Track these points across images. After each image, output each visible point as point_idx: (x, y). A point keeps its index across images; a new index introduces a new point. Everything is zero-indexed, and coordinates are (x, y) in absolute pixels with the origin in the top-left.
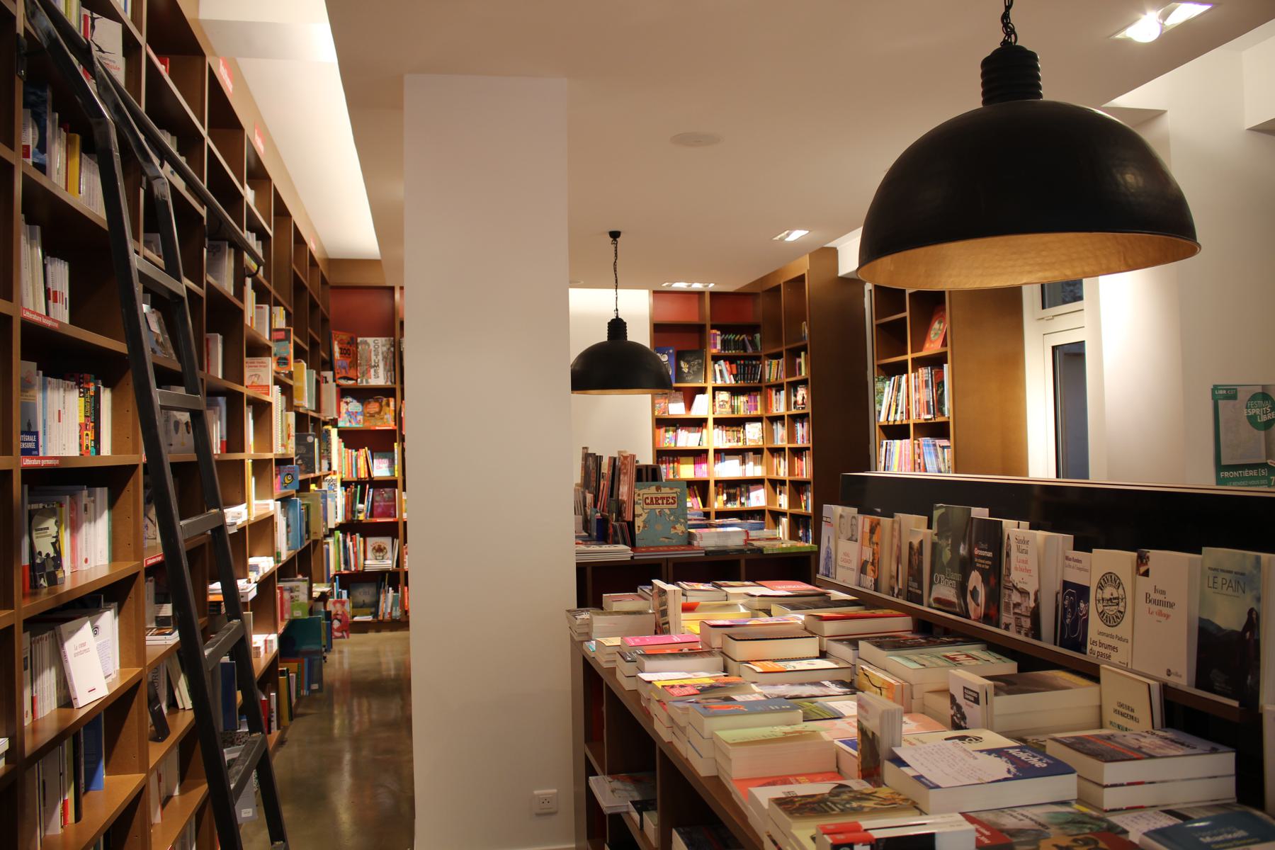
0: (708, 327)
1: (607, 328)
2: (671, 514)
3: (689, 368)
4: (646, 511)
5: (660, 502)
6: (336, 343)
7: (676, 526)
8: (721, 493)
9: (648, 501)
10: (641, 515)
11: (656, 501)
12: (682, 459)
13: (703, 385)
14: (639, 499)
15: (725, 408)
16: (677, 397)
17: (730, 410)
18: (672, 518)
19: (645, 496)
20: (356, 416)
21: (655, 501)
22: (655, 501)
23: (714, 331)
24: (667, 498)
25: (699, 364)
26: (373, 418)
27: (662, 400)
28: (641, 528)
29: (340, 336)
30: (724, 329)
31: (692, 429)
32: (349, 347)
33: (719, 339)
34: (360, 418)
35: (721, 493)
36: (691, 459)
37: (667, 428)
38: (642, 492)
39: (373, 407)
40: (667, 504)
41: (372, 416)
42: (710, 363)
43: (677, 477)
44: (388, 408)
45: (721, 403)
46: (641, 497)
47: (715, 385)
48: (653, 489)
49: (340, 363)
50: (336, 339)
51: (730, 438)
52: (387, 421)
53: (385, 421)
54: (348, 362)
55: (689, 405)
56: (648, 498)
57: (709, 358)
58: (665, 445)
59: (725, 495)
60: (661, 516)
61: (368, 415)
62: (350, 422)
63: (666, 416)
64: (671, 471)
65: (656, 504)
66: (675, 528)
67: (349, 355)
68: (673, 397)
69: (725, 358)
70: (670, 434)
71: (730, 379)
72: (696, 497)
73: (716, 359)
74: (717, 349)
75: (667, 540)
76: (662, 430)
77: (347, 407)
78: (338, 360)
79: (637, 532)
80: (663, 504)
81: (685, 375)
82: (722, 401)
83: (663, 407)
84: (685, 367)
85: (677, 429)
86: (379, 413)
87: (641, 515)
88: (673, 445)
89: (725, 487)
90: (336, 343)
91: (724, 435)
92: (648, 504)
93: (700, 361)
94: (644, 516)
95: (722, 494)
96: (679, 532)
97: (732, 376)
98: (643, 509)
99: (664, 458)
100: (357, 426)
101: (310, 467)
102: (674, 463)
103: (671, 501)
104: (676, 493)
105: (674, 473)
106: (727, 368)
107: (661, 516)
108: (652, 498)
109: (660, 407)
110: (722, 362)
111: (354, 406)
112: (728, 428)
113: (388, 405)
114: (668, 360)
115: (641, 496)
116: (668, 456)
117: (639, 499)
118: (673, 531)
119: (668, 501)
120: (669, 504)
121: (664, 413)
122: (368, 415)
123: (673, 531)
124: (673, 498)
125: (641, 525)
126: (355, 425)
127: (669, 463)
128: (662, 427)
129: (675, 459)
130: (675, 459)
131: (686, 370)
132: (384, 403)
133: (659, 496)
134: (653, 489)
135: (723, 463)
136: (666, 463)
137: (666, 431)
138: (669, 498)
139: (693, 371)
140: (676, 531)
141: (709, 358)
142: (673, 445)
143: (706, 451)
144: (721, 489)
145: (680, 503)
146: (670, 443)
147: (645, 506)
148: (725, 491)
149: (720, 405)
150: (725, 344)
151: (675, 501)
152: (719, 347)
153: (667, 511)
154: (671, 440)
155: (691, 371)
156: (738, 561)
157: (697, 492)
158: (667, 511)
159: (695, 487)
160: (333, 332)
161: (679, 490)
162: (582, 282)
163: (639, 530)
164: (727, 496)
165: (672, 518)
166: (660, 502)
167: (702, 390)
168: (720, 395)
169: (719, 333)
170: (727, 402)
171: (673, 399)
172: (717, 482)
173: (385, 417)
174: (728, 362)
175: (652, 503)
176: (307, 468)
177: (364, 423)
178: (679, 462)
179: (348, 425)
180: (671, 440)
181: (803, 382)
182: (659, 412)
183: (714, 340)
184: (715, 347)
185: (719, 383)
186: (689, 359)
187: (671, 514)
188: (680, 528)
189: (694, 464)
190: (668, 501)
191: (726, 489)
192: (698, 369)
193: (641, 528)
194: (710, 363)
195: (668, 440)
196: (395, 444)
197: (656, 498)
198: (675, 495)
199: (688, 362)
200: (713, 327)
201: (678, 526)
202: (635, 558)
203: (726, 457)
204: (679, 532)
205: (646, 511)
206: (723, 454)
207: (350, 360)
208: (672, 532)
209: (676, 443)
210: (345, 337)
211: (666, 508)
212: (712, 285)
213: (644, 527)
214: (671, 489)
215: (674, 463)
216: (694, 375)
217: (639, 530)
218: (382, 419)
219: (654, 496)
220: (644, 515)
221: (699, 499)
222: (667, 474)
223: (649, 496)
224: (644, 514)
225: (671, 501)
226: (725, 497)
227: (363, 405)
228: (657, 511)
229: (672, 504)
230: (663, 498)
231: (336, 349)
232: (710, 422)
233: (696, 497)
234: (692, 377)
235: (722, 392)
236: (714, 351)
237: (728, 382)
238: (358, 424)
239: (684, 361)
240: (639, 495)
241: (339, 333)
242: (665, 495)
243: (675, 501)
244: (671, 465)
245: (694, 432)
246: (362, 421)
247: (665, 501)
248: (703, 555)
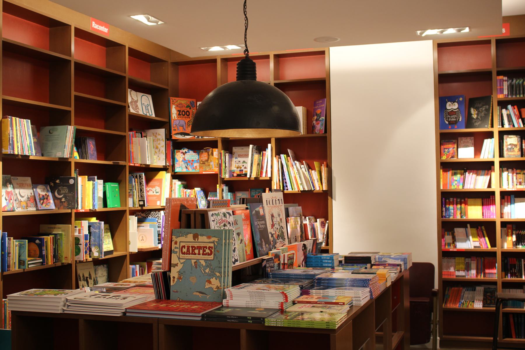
0: (494, 74)
1: (257, 72)
2: (207, 266)
3: (478, 114)
4: (182, 261)
5: (196, 251)
6: (174, 106)
7: (211, 280)
8: (510, 233)
9: (185, 250)
10: (177, 265)
11: (193, 250)
12: (470, 201)
13: (490, 129)
14: (176, 248)
15: (513, 151)
16: (468, 142)
17: (519, 153)
18: (207, 271)
19: (182, 244)
20: (192, 164)
21: (191, 250)
22: (191, 250)
23: (501, 77)
24: (204, 247)
25: (486, 110)
26: (204, 165)
27: (450, 146)
28: (176, 280)
29: (179, 101)
30: (511, 74)
31: (481, 172)
32: (188, 109)
33: (506, 85)
34: (196, 164)
35: (510, 233)
36: (479, 201)
37: (456, 171)
38: (179, 240)
39: (204, 156)
40: (203, 254)
41: (204, 163)
42: (496, 109)
43: (464, 218)
44: (212, 157)
45: (510, 147)
46: (178, 246)
47: (502, 129)
48: (190, 237)
49: (177, 122)
50: (173, 104)
51: (521, 180)
52: (212, 167)
53: (211, 167)
54: (187, 122)
55: (478, 150)
56: (184, 247)
57: (495, 104)
58: (453, 188)
59: (514, 236)
60: (196, 267)
61: (202, 162)
62: (187, 168)
63: (455, 160)
64: (458, 212)
65: (192, 254)
66: (210, 282)
67: (189, 115)
68: (464, 142)
69: (513, 103)
70: (458, 177)
71: (518, 123)
72: (484, 237)
73: (503, 104)
74: (504, 94)
75: (200, 295)
76: (449, 173)
77: (183, 156)
78: (175, 120)
79: (172, 284)
80: (199, 254)
81: (474, 121)
82: (510, 144)
83: (451, 152)
84: (474, 113)
85: (465, 172)
86: (207, 160)
87: (177, 265)
88: (461, 187)
89: (514, 228)
90: (174, 106)
91: (515, 178)
92: (184, 253)
93: (487, 107)
94: (180, 266)
95: (512, 235)
96: (214, 287)
97: (520, 120)
98: (179, 258)
99: (451, 199)
100: (194, 171)
101: (71, 204)
102: (461, 204)
103: (207, 251)
104: (213, 242)
105: (461, 213)
106: (514, 113)
107: (196, 267)
108: (188, 247)
109: (448, 152)
110: (510, 107)
111: (191, 155)
112: (518, 171)
113: (212, 154)
114: (458, 108)
115: (178, 243)
116: (457, 198)
117: (176, 248)
118: (207, 286)
119: (204, 251)
120: (206, 254)
121: (453, 157)
122: (202, 162)
123: (207, 286)
124: (210, 247)
125: (176, 276)
126: (191, 170)
127: (457, 204)
128: (449, 171)
129: (447, 201)
130: (463, 200)
131: (475, 116)
132: (210, 153)
133: (196, 245)
134: (190, 237)
135: (512, 205)
136: (453, 204)
137: (455, 174)
138: (206, 247)
139: (481, 117)
140: (211, 286)
141: (495, 104)
142: (461, 187)
143: (493, 193)
144: (510, 231)
145: (216, 253)
146: (458, 186)
147: (182, 256)
148: (514, 232)
149: (508, 149)
150: (511, 88)
151: (211, 251)
152: (506, 92)
153: (203, 262)
154: (459, 182)
155: (479, 117)
156: (238, 331)
157: (485, 232)
158: (203, 262)
159: (483, 228)
160: (171, 98)
161: (216, 239)
162: (339, 40)
163: (174, 281)
164: (517, 238)
165: (207, 271)
166: (196, 251)
167: (490, 135)
168: (508, 139)
169: (505, 78)
170: (516, 146)
171: (463, 144)
172: (504, 224)
173: (211, 164)
174: (516, 107)
175: (188, 253)
176: (69, 204)
177: (200, 169)
178: (466, 204)
179: (185, 170)
180: (459, 182)
181: (317, 115)
182: (447, 157)
183: (500, 86)
184: (502, 92)
185: (507, 126)
186: (478, 105)
187: (207, 266)
188: (215, 282)
189: (483, 205)
190: (204, 251)
191: (516, 230)
192: (485, 114)
193: (176, 280)
194: (496, 109)
195: (456, 182)
196: (218, 185)
197: (192, 247)
198: (212, 245)
199: (477, 109)
200: (499, 73)
201: (213, 280)
202: (128, 314)
203: (516, 199)
204: (214, 287)
205: (182, 261)
206: (512, 196)
207: (189, 120)
208: (207, 287)
209: (463, 186)
210: (184, 101)
211: (202, 259)
212: (467, 30)
213: (179, 278)
214: (209, 237)
215: (461, 204)
216: (481, 120)
217: (174, 281)
218: (209, 165)
219: (191, 245)
220: (179, 264)
221: (487, 239)
222: (455, 214)
223: (186, 245)
224: (179, 263)
225: (207, 251)
226: (514, 238)
227: (198, 155)
228: (193, 261)
229: (209, 254)
230: (199, 248)
231: (174, 111)
232: (497, 166)
233: (484, 237)
234: (479, 123)
235: (510, 136)
236: (501, 96)
237: (516, 126)
238: (195, 169)
239: (474, 108)
240: (176, 243)
241: (178, 99)
242: (202, 245)
243: (211, 251)
244: (459, 206)
245: (484, 175)
246: (198, 167)
247: (201, 252)
248: (199, 319)
